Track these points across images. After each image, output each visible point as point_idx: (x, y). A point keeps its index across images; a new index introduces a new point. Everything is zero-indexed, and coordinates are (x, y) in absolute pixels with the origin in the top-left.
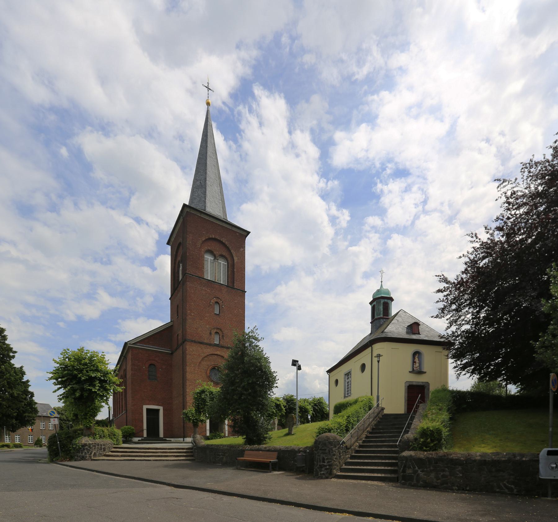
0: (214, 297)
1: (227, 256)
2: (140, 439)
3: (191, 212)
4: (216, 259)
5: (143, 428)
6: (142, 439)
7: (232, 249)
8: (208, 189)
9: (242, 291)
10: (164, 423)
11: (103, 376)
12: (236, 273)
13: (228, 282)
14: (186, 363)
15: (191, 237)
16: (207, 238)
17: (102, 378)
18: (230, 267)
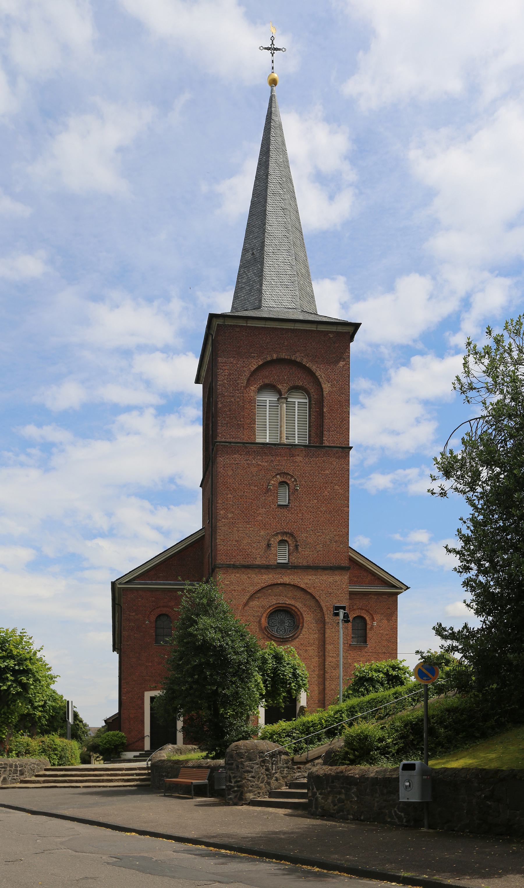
1: (307, 387)
2: (137, 753)
3: (226, 323)
4: (283, 398)
5: (144, 733)
6: (140, 754)
7: (318, 369)
8: (268, 262)
9: (342, 448)
11: (19, 664)
12: (327, 415)
17: (17, 668)
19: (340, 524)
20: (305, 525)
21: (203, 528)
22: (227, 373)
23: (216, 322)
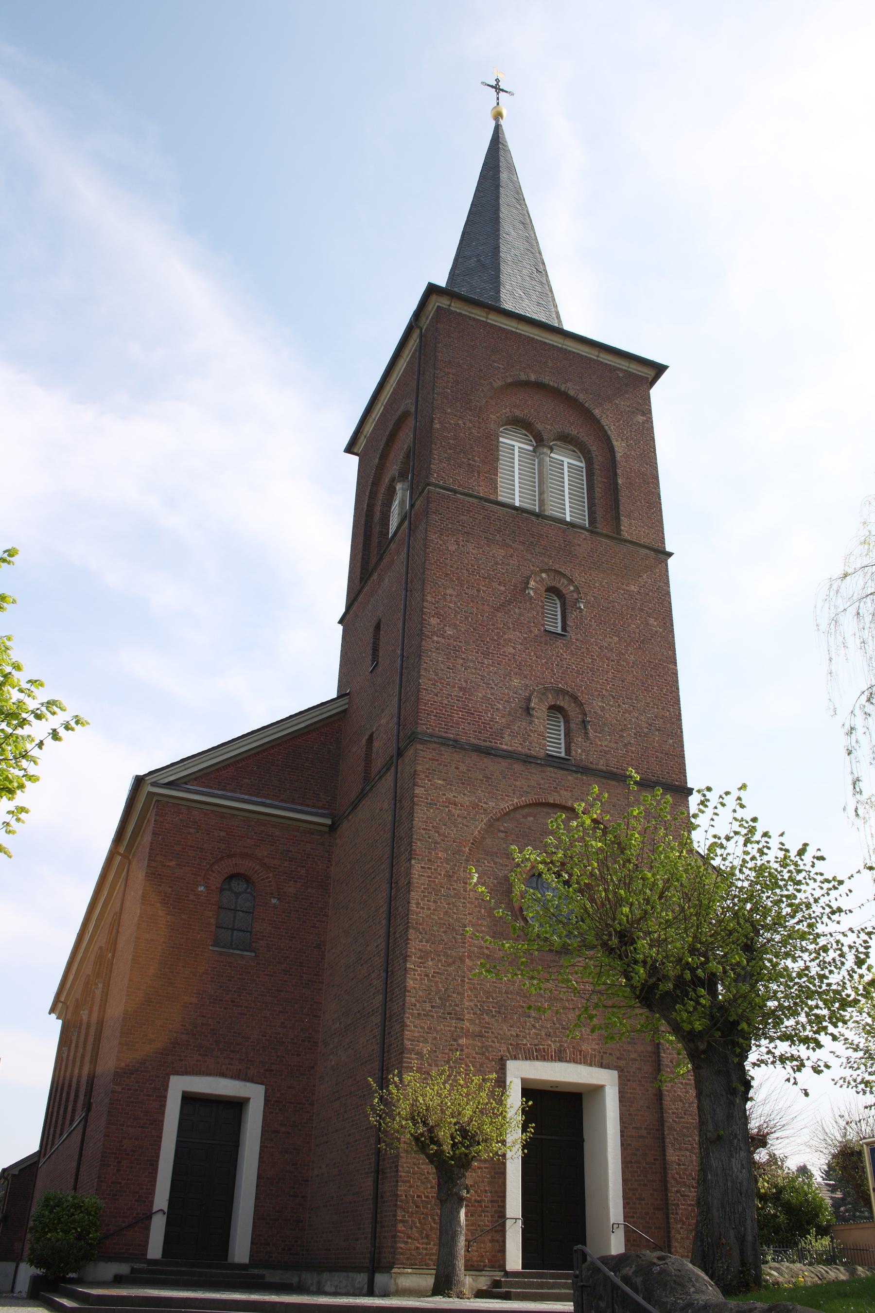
0: (542, 571)
3: (452, 309)
5: (152, 1202)
10: (259, 1177)
12: (624, 494)
13: (592, 513)
14: (410, 844)
15: (451, 376)
16: (509, 380)
18: (597, 472)
19: (664, 694)
20: (598, 682)
21: (339, 697)
22: (453, 378)
23: (436, 302)
